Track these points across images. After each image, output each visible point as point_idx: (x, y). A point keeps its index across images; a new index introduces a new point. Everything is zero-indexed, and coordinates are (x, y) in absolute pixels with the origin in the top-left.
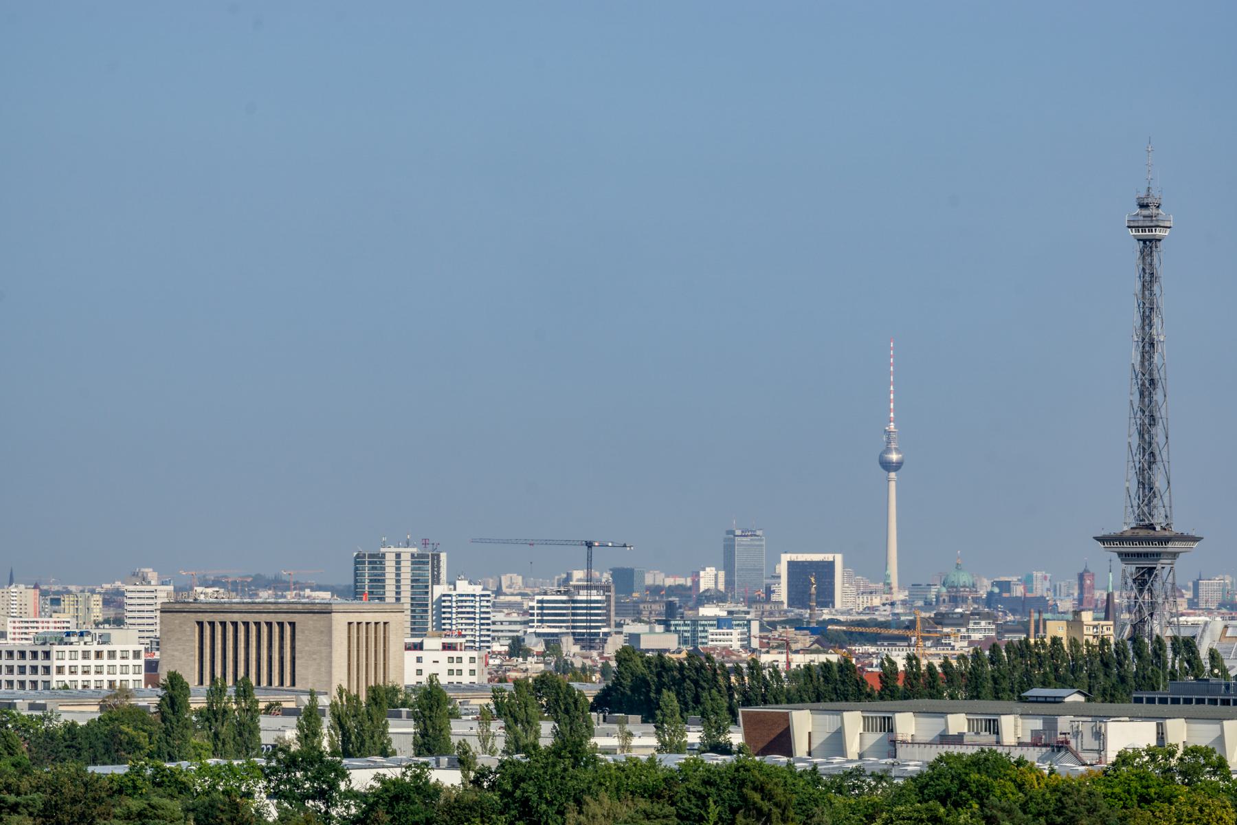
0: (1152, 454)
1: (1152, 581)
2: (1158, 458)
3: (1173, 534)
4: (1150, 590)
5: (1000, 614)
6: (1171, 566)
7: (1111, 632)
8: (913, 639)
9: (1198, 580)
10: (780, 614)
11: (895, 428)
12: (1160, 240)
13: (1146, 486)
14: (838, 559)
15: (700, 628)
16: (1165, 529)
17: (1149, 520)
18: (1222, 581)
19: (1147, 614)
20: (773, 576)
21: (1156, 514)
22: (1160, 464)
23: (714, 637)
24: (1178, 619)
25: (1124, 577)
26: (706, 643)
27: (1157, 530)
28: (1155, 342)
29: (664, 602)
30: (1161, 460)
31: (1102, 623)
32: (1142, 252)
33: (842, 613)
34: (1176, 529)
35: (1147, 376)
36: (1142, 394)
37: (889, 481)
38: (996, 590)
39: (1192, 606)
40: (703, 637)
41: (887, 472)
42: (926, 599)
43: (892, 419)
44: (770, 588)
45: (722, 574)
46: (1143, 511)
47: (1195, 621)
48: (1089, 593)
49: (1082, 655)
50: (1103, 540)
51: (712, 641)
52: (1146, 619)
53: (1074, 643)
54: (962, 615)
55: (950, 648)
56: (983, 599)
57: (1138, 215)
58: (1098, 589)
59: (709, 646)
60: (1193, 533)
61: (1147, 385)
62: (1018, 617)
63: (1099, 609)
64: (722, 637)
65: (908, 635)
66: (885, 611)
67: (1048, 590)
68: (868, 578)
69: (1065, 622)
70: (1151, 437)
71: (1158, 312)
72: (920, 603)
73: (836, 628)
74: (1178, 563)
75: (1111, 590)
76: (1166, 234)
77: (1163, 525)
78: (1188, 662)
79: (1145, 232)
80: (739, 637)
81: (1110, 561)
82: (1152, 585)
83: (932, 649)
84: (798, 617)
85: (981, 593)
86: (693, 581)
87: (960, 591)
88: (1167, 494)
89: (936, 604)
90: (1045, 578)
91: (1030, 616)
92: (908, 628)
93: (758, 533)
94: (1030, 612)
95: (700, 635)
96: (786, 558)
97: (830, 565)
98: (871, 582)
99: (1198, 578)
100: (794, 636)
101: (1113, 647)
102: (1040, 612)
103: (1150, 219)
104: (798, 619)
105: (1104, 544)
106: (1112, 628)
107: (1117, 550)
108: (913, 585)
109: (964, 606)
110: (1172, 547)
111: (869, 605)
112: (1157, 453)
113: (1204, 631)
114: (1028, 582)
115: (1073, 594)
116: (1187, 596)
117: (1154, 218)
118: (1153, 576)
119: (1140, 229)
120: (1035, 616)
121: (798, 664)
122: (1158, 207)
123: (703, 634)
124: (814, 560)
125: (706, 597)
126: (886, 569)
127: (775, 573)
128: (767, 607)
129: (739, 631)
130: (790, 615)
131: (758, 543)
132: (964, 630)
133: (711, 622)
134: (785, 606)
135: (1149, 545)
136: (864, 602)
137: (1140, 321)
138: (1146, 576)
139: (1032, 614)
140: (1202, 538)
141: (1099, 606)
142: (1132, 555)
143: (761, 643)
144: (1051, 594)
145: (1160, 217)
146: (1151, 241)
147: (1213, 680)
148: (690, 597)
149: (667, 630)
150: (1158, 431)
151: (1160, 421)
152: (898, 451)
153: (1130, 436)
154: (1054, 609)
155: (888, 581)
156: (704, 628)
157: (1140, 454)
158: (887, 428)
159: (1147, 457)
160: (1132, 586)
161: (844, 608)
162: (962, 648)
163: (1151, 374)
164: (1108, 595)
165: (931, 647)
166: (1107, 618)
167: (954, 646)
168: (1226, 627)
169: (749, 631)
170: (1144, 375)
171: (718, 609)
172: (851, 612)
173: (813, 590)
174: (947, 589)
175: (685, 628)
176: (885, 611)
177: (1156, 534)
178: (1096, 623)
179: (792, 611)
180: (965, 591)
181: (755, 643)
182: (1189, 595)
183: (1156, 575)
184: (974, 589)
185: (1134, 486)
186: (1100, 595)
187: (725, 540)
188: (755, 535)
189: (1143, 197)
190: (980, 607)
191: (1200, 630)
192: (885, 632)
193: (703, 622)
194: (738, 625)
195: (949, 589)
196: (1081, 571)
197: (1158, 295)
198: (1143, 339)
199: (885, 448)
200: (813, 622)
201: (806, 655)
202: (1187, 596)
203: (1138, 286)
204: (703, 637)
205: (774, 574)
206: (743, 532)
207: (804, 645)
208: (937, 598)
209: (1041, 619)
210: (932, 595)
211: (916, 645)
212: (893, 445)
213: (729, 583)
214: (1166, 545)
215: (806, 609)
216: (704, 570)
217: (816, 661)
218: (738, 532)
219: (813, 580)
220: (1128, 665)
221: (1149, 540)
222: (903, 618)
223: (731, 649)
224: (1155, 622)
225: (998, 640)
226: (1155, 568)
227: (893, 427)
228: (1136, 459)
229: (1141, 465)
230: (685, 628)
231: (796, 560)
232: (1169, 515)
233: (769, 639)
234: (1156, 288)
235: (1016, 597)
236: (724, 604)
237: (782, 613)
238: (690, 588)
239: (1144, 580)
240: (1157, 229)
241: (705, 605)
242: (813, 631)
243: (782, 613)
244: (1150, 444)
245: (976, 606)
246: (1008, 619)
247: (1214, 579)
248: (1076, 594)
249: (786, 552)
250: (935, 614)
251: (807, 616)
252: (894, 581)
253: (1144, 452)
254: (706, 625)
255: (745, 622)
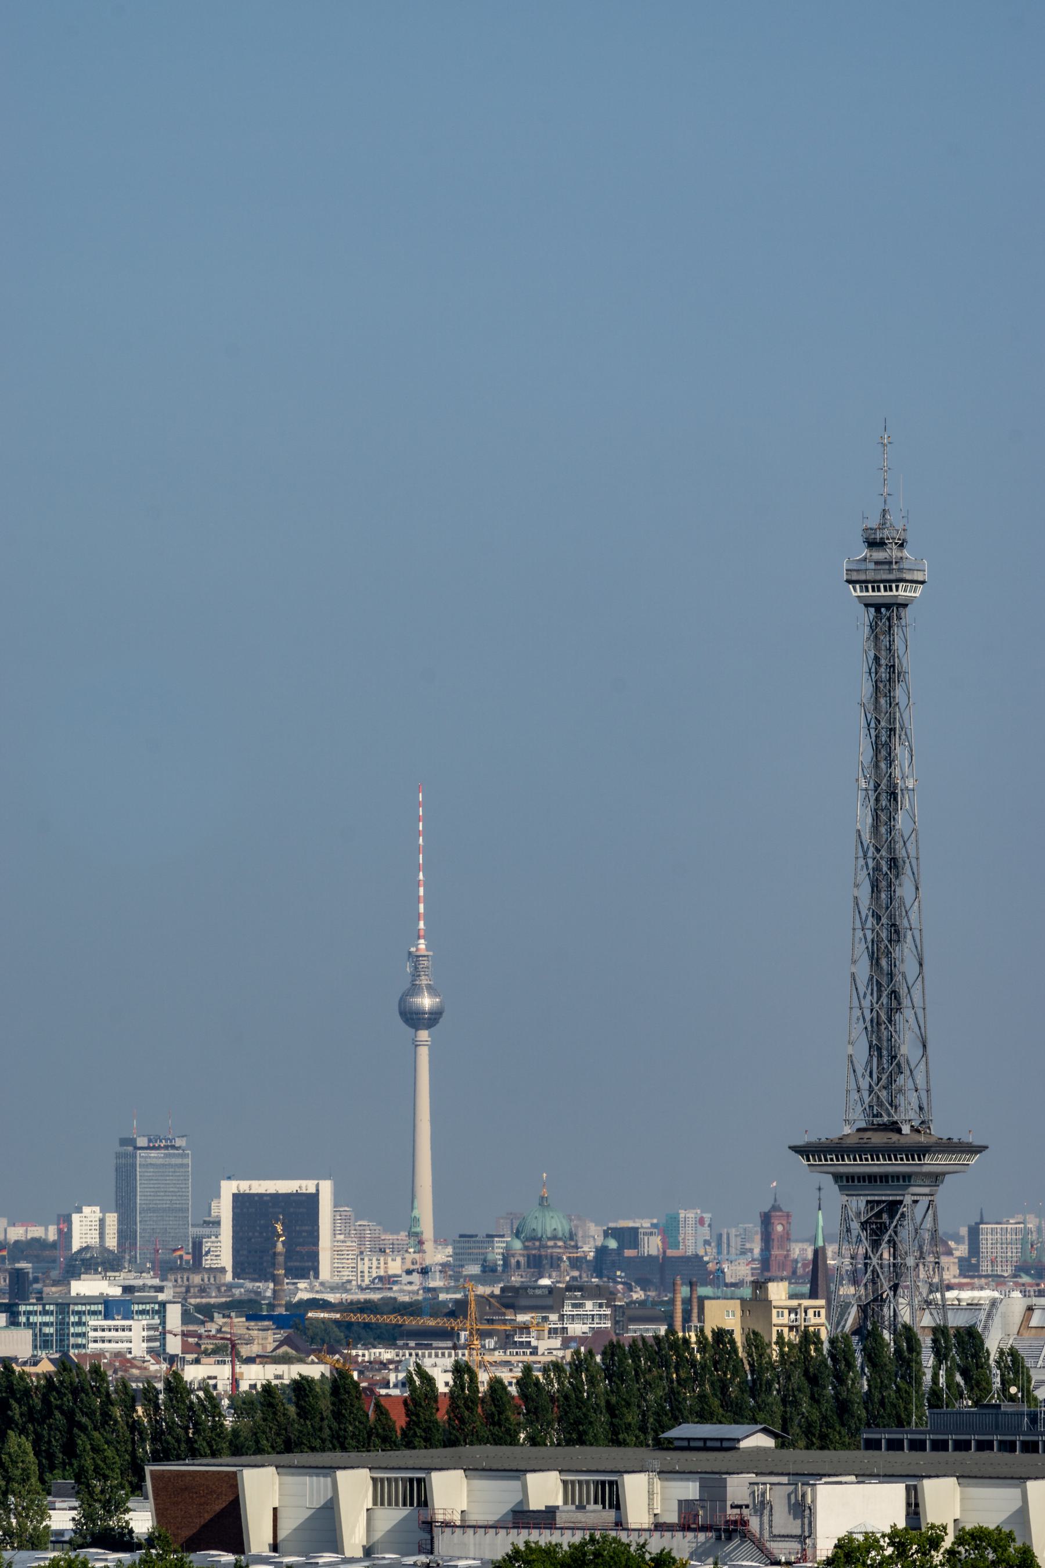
0: (894, 994)
1: (896, 1227)
2: (906, 1002)
3: (933, 1140)
4: (893, 1243)
5: (620, 1287)
6: (930, 1198)
7: (823, 1319)
8: (463, 1335)
9: (978, 1224)
10: (219, 1290)
11: (427, 949)
12: (905, 606)
13: (885, 1053)
14: (326, 1190)
15: (73, 1319)
16: (918, 1131)
17: (889, 1115)
18: (1022, 1226)
19: (886, 1286)
20: (205, 1222)
21: (902, 1105)
22: (908, 1013)
23: (99, 1334)
24: (943, 1296)
25: (846, 1219)
26: (84, 1346)
27: (903, 1132)
28: (898, 791)
29: (6, 1270)
30: (910, 1005)
31: (806, 1303)
32: (873, 627)
33: (333, 1289)
34: (939, 1131)
35: (883, 853)
36: (875, 887)
37: (417, 1046)
38: (613, 1244)
39: (969, 1271)
40: (78, 1335)
41: (414, 1030)
42: (485, 1260)
43: (422, 933)
44: (201, 1244)
45: (112, 1219)
46: (878, 1097)
47: (973, 1298)
48: (781, 1247)
49: (770, 1363)
50: (805, 1151)
51: (95, 1341)
52: (884, 1296)
53: (755, 1341)
54: (551, 1290)
55: (528, 1351)
56: (590, 1261)
57: (865, 559)
58: (797, 1241)
59: (88, 1351)
60: (970, 1139)
61: (885, 869)
62: (652, 1294)
63: (801, 1277)
64: (113, 1333)
65: (453, 1329)
66: (410, 1283)
67: (707, 1243)
68: (379, 1224)
69: (738, 1302)
70: (892, 964)
71: (903, 737)
72: (475, 1269)
73: (322, 1315)
74: (944, 1192)
75: (820, 1243)
76: (917, 595)
77: (915, 1123)
78: (965, 1373)
79: (879, 590)
80: (145, 1334)
81: (820, 1189)
82: (896, 1233)
83: (496, 1353)
84: (253, 1296)
85: (586, 1249)
86: (60, 1232)
87: (548, 1247)
88: (922, 1066)
89: (503, 1271)
90: (701, 1222)
91: (674, 1292)
92: (452, 1314)
93: (178, 1142)
94: (674, 1284)
95: (72, 1330)
96: (229, 1188)
97: (313, 1199)
98: (385, 1231)
99: (978, 1221)
100: (245, 1331)
101: (826, 1346)
102: (691, 1285)
103: (887, 567)
104: (250, 1301)
105: (808, 1160)
106: (823, 1312)
107: (832, 1169)
108: (461, 1236)
109: (554, 1274)
110: (932, 1163)
111: (382, 1273)
112: (903, 992)
113: (989, 1315)
114: (669, 1230)
115: (751, 1250)
116: (957, 1253)
117: (894, 567)
118: (897, 1217)
119: (870, 586)
120: (684, 1291)
121: (253, 1382)
122: (902, 545)
123: (79, 1330)
124: (280, 1192)
125: (82, 1260)
126: (412, 1208)
127: (210, 1215)
128: (196, 1279)
129: (145, 1322)
130: (237, 1292)
131: (179, 1161)
132: (553, 1317)
133: (93, 1308)
134: (229, 1277)
135: (890, 1159)
136: (372, 1267)
137: (870, 753)
138: (885, 1216)
139: (678, 1288)
140: (987, 1147)
141: (800, 1271)
142: (859, 1178)
143: (184, 1344)
144: (712, 1250)
145: (905, 565)
146: (888, 606)
147: (1007, 1407)
148: (54, 1261)
149: (13, 1323)
150: (905, 953)
151: (909, 933)
152: (432, 990)
153: (857, 886)
154: (717, 1279)
155: (414, 1230)
156: (80, 1318)
157: (872, 994)
158: (413, 949)
159: (884, 1000)
160: (859, 1235)
161: (336, 1279)
162: (550, 1351)
163: (891, 849)
164: (816, 1252)
165: (494, 1349)
166: (813, 1295)
167: (536, 1348)
168: (1030, 1309)
169: (163, 1323)
170: (878, 850)
171: (106, 1283)
172: (348, 1287)
173: (280, 1247)
174: (523, 1243)
175: (47, 1319)
176: (410, 1283)
177: (903, 1140)
178: (794, 1303)
179: (241, 1286)
180: (555, 1246)
181: (174, 1346)
182: (961, 1250)
183: (903, 1215)
184: (573, 1243)
185: (861, 1052)
186: (801, 1251)
187: (118, 1156)
188: (173, 1147)
189: (875, 527)
190: (584, 1275)
191: (983, 1316)
192: (411, 1322)
193: (79, 1308)
194: (142, 1312)
195: (527, 1244)
196: (767, 1211)
197: (902, 706)
198: (877, 786)
199: (409, 985)
200: (280, 1305)
201: (267, 1366)
202: (957, 1253)
203: (866, 688)
204: (78, 1335)
205: (207, 1219)
206: (150, 1141)
207: (264, 1347)
208: (506, 1259)
209: (695, 1296)
210: (496, 1253)
211: (468, 1346)
212: (424, 981)
213: (126, 1235)
214: (920, 1160)
215: (266, 1281)
216: (79, 1210)
217: (286, 1376)
218: (142, 1142)
219: (279, 1228)
220: (852, 1380)
221: (890, 1152)
222: (442, 1297)
223: (129, 1356)
224: (901, 1300)
225: (617, 1335)
226: (901, 1202)
227: (422, 947)
228: (866, 1003)
229: (875, 1014)
230: (47, 1319)
231: (247, 1191)
232: (925, 1106)
233: (200, 1337)
234: (899, 693)
235: (649, 1256)
236: (117, 1274)
237: (223, 1289)
238: (54, 1245)
239: (881, 1223)
240: (901, 585)
241: (83, 1276)
242: (280, 1322)
243: (223, 1289)
244: (891, 975)
245: (576, 1274)
246: (635, 1296)
247: (1008, 1223)
248: (757, 1251)
249: (229, 1178)
250: (503, 1290)
251: (269, 1294)
252: (427, 1228)
253: (879, 991)
254: (84, 1313)
255: (157, 1307)
